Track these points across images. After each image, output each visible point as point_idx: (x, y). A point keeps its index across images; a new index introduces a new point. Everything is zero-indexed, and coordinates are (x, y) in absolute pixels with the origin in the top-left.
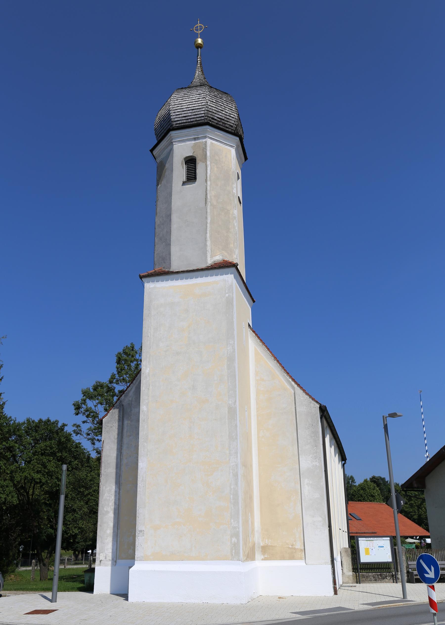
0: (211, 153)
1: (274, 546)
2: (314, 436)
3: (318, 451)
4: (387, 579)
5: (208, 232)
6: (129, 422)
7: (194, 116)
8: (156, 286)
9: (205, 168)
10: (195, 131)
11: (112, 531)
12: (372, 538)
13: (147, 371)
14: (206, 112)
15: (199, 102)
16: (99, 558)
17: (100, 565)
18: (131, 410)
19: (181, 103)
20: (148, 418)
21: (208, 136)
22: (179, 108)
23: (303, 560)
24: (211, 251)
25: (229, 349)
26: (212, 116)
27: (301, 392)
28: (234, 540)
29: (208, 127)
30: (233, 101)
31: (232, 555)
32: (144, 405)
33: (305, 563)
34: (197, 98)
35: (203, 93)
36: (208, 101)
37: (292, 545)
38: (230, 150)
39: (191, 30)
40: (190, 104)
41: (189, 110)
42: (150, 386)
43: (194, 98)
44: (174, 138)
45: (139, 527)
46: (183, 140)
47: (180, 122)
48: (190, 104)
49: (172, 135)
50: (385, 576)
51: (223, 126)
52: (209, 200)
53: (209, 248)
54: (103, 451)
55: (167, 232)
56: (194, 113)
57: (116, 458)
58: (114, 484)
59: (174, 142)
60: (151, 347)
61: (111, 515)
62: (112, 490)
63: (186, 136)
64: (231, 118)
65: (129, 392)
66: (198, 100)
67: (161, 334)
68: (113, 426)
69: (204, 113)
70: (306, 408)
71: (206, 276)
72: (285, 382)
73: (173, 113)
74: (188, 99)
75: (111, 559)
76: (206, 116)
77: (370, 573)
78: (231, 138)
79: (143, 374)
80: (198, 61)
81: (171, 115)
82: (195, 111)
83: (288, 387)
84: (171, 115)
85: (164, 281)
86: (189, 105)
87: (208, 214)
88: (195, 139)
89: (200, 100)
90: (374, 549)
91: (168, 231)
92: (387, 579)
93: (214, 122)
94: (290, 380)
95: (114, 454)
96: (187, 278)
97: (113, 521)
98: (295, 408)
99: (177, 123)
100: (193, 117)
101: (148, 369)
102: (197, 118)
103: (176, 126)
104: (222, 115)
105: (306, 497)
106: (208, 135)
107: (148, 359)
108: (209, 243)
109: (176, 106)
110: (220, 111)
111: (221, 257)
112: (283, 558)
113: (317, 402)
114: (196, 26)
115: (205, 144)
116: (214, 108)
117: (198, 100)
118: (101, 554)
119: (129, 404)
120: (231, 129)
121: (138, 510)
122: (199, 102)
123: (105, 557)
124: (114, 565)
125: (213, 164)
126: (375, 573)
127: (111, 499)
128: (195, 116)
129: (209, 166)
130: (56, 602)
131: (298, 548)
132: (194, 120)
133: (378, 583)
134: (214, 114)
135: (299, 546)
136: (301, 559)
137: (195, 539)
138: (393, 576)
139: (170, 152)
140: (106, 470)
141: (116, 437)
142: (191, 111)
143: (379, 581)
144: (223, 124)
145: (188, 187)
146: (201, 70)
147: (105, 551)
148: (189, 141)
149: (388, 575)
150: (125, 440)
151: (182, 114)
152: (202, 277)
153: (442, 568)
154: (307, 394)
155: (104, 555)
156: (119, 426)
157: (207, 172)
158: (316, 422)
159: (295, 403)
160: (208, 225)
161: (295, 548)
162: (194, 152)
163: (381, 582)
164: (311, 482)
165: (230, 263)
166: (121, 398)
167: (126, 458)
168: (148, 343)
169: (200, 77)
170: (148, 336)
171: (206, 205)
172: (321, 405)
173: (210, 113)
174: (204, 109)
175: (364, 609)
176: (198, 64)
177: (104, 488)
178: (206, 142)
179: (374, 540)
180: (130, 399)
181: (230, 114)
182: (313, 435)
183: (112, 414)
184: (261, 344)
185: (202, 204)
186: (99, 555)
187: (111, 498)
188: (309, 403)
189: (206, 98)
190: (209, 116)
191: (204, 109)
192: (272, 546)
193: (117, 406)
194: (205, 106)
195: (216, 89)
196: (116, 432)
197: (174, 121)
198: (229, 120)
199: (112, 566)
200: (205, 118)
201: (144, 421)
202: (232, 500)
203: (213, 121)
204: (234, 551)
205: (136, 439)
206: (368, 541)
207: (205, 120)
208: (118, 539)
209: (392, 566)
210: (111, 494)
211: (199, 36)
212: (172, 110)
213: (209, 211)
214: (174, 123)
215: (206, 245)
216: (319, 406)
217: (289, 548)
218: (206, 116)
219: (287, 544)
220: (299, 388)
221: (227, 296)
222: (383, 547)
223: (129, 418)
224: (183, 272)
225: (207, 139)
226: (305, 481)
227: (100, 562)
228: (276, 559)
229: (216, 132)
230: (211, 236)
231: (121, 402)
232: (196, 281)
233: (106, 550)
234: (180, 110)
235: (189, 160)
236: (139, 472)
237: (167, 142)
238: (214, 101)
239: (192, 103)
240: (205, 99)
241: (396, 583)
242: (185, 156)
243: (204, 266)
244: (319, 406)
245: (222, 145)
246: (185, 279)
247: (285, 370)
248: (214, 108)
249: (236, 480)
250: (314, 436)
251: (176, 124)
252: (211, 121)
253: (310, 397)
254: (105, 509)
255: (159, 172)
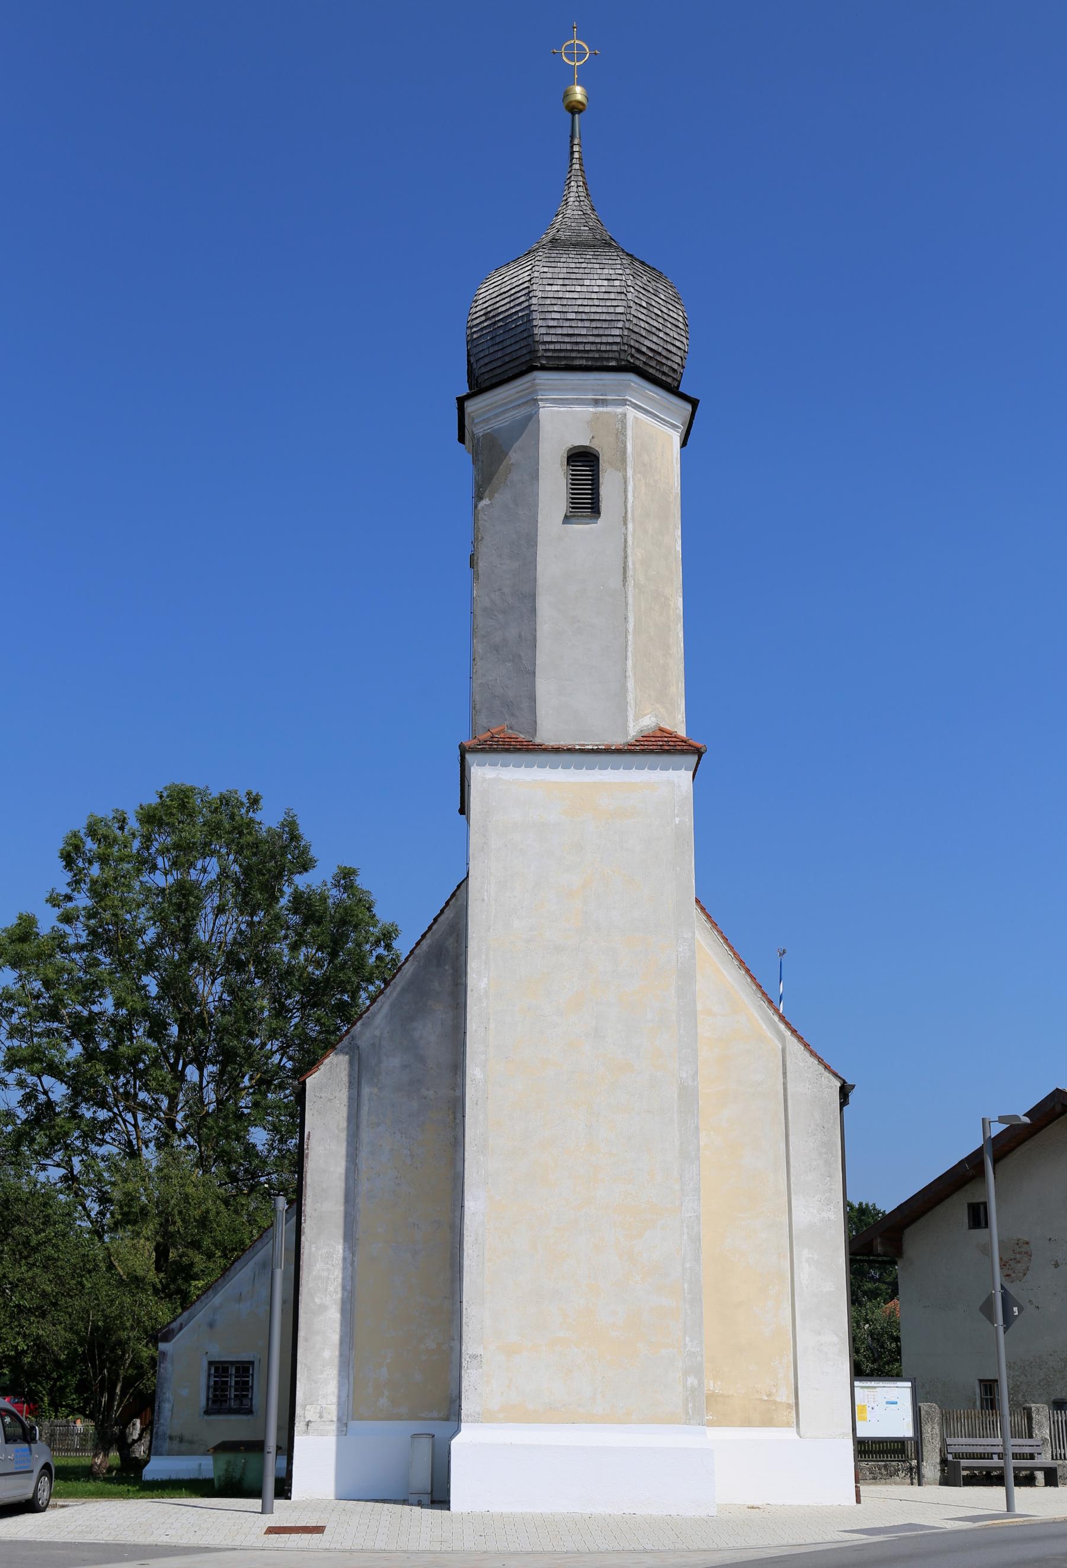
0: (634, 446)
1: (728, 1396)
2: (826, 1153)
3: (833, 1187)
4: (898, 1476)
5: (629, 654)
6: (375, 1090)
7: (594, 338)
8: (500, 776)
9: (624, 486)
10: (599, 382)
11: (337, 1353)
12: (873, 1383)
13: (483, 985)
14: (626, 333)
15: (608, 303)
16: (305, 1417)
17: (306, 1432)
18: (380, 1062)
19: (560, 295)
20: (487, 1098)
21: (630, 401)
22: (556, 308)
23: (793, 1427)
24: (636, 704)
25: (680, 949)
26: (637, 345)
27: (800, 1048)
28: (692, 1380)
29: (632, 378)
30: (679, 299)
31: (687, 1413)
32: (476, 1066)
33: (798, 1433)
34: (603, 289)
35: (619, 277)
36: (631, 304)
37: (769, 1395)
38: (669, 435)
39: (554, 53)
40: (585, 302)
41: (582, 320)
42: (491, 1021)
43: (596, 289)
44: (541, 390)
45: (470, 1346)
46: (567, 399)
47: (558, 347)
48: (585, 302)
49: (537, 381)
50: (895, 1470)
51: (657, 370)
52: (630, 573)
53: (630, 696)
54: (309, 1159)
55: (520, 636)
56: (594, 329)
57: (343, 1177)
58: (341, 1241)
59: (542, 400)
60: (490, 928)
61: (334, 1315)
62: (335, 1256)
63: (573, 390)
64: (674, 350)
65: (374, 1015)
66: (606, 296)
67: (515, 897)
68: (335, 1098)
69: (621, 334)
70: (810, 1086)
71: (628, 767)
72: (761, 1021)
73: (540, 319)
74: (578, 289)
75: (335, 1419)
76: (624, 344)
77: (863, 1461)
78: (676, 405)
79: (472, 990)
80: (572, 153)
81: (535, 323)
82: (599, 324)
83: (770, 1034)
84: (535, 323)
85: (520, 767)
86: (582, 305)
87: (630, 608)
88: (596, 402)
89: (612, 296)
90: (876, 1408)
91: (523, 635)
92: (898, 1476)
93: (640, 360)
94: (776, 1019)
95: (339, 1168)
96: (578, 767)
97: (338, 1330)
98: (785, 1084)
99: (547, 347)
100: (591, 339)
101: (485, 980)
102: (601, 343)
103: (545, 355)
104: (658, 342)
105: (805, 1289)
106: (629, 398)
107: (484, 957)
108: (630, 684)
109: (548, 302)
110: (654, 330)
111: (653, 719)
112: (747, 1423)
113: (835, 1075)
114: (568, 43)
115: (622, 422)
116: (642, 324)
117: (606, 296)
118: (308, 1407)
119: (373, 1045)
120: (671, 378)
121: (466, 1309)
122: (608, 303)
123: (318, 1415)
124: (344, 1433)
125: (639, 475)
126: (873, 1463)
127: (333, 1277)
128: (598, 340)
129: (631, 482)
130: (273, 1513)
131: (781, 1402)
132: (593, 348)
133: (878, 1484)
134: (642, 340)
135: (784, 1396)
136: (788, 1425)
137: (604, 1377)
138: (911, 1469)
139: (528, 423)
140: (319, 1205)
141: (344, 1124)
142: (587, 324)
143: (883, 1481)
144: (657, 364)
145: (578, 528)
146: (583, 183)
147: (318, 1400)
148: (579, 404)
149: (900, 1467)
150: (365, 1135)
151: (562, 327)
152: (615, 767)
153: (1016, 1454)
154: (813, 1053)
155: (315, 1408)
156: (350, 1098)
157: (626, 498)
158: (832, 1121)
159: (785, 1074)
160: (630, 637)
161: (775, 1401)
162: (593, 437)
163: (886, 1484)
164: (816, 1257)
165: (682, 741)
166: (352, 1030)
167: (368, 1180)
168: (484, 917)
169: (582, 203)
170: (483, 900)
171: (624, 585)
172: (844, 1082)
173: (634, 336)
174: (620, 325)
175: (960, 1528)
176: (574, 161)
177: (314, 1249)
178: (625, 415)
179: (878, 1387)
180: (377, 1033)
181: (674, 338)
182: (824, 1150)
183: (331, 1067)
184: (709, 925)
185: (615, 582)
186: (304, 1408)
187: (333, 1274)
188: (817, 1075)
189: (626, 295)
190: (632, 343)
191: (620, 325)
192: (722, 1396)
193: (344, 1048)
194: (623, 317)
195: (642, 263)
196: (344, 1112)
197: (541, 341)
198: (669, 356)
199: (337, 1436)
200: (623, 348)
201: (476, 1104)
202: (686, 1295)
203: (638, 356)
204: (690, 1405)
205: (394, 1133)
206: (866, 1390)
207: (621, 352)
208: (351, 1371)
209: (910, 1448)
210: (333, 1265)
211: (576, 76)
212: (536, 311)
213: (630, 600)
214: (542, 347)
215: (624, 689)
216: (839, 1085)
217: (762, 1400)
218: (624, 344)
219: (758, 1392)
220: (794, 1040)
221: (677, 822)
222: (896, 1403)
223: (375, 1080)
224: (570, 751)
225: (627, 407)
226: (803, 1254)
227: (307, 1425)
228: (731, 1424)
229: (651, 391)
230: (634, 666)
231: (353, 1038)
232: (602, 775)
233: (322, 1398)
234: (557, 314)
235: (577, 453)
236: (468, 1223)
237: (517, 393)
238: (644, 304)
239: (590, 302)
240: (623, 297)
241: (920, 1484)
242: (569, 445)
243: (617, 740)
244: (840, 1085)
245: (655, 422)
246: (574, 768)
247: (764, 994)
248: (642, 324)
249: (696, 1251)
250: (826, 1153)
251: (546, 350)
252: (634, 357)
253: (821, 1061)
254: (317, 1300)
255: (482, 462)
